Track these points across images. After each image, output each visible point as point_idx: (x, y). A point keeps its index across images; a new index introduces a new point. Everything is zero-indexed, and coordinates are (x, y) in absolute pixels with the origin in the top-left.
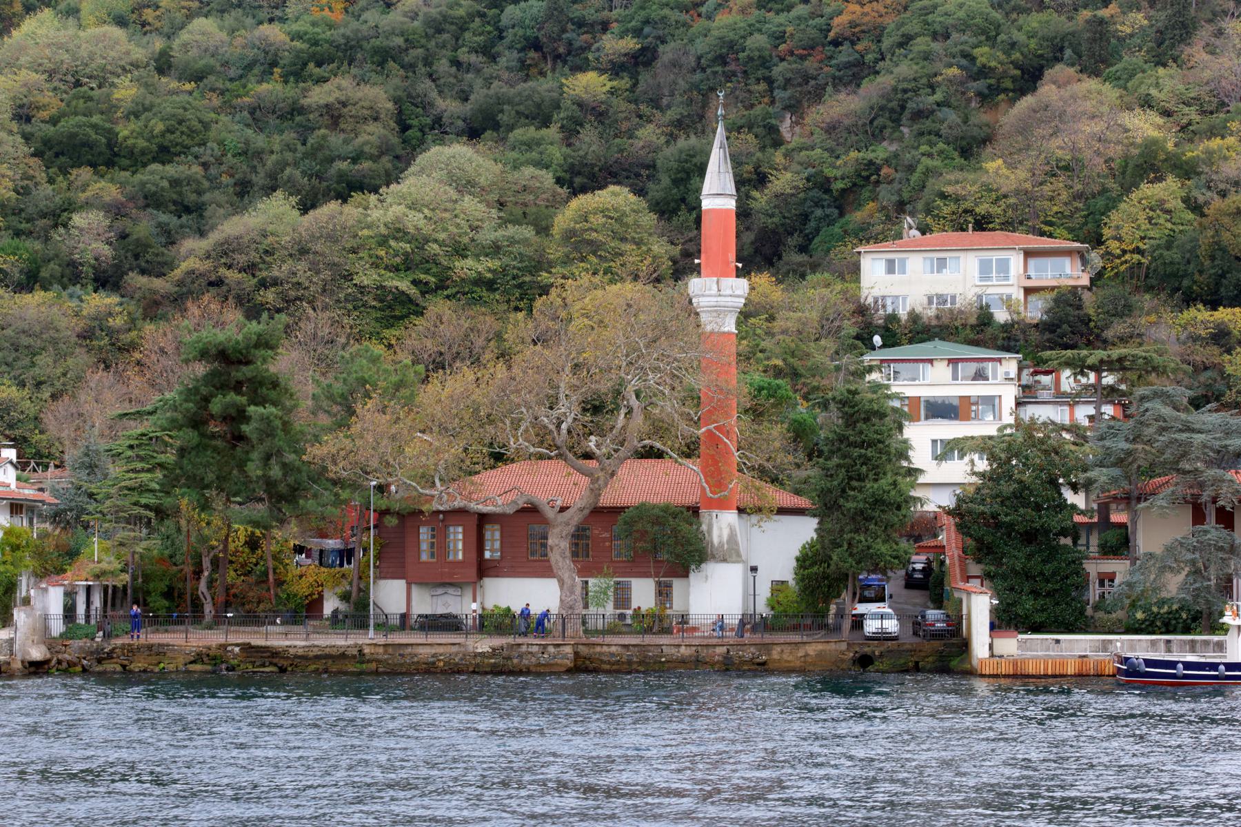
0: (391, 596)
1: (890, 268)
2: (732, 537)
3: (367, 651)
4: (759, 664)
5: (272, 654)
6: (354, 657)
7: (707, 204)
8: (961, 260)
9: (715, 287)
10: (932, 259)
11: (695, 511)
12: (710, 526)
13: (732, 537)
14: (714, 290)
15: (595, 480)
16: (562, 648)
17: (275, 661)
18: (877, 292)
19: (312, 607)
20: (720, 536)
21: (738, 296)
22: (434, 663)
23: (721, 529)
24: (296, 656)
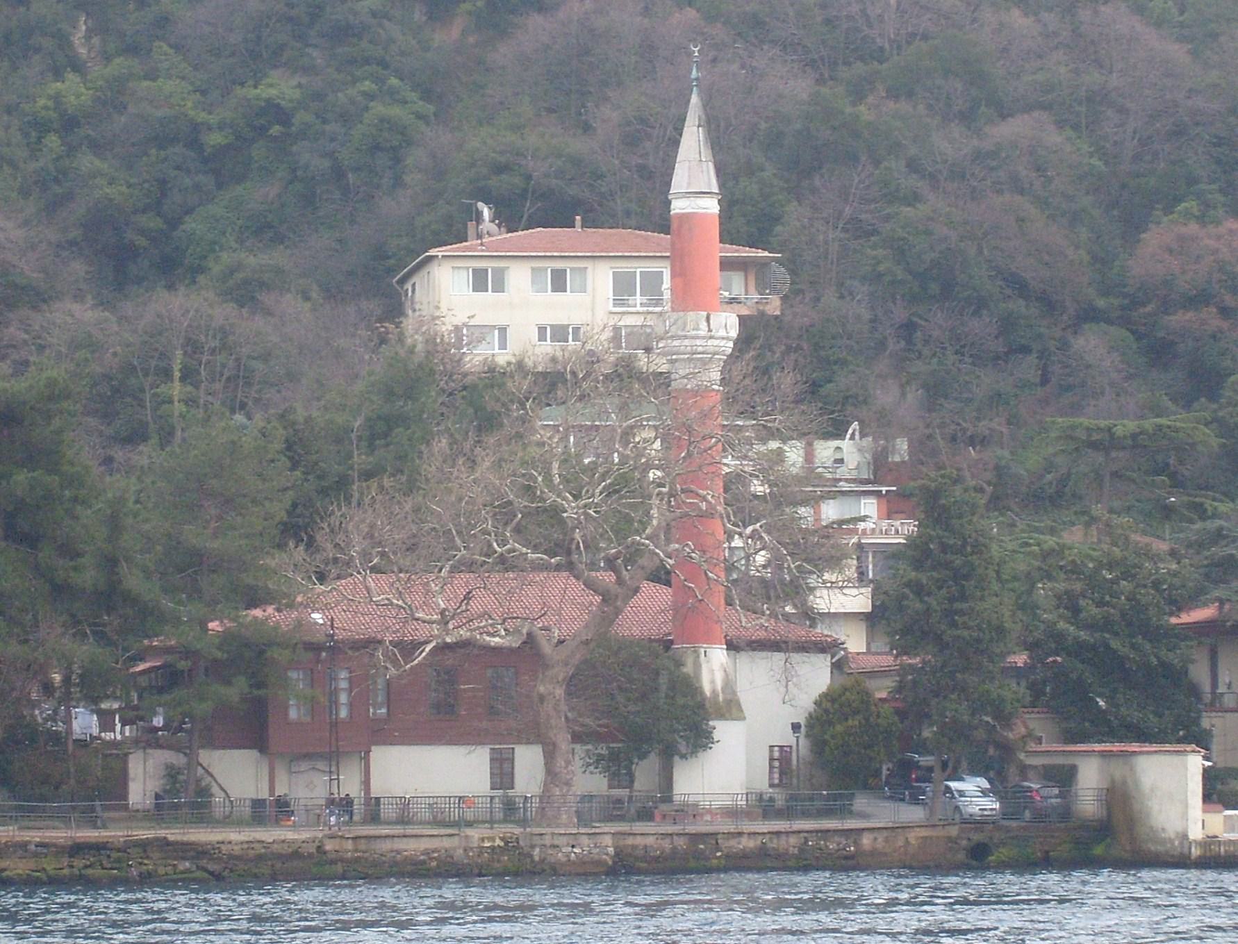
0: (237, 774)
1: (480, 281)
2: (729, 685)
3: (329, 846)
4: (846, 858)
5: (199, 852)
6: (310, 856)
7: (679, 206)
8: (590, 271)
9: (704, 325)
10: (468, 268)
11: (668, 645)
12: (697, 666)
13: (729, 685)
14: (703, 331)
15: (607, 598)
16: (599, 839)
17: (204, 863)
18: (460, 319)
19: (115, 788)
20: (713, 682)
21: (728, 339)
22: (424, 862)
23: (712, 671)
24: (231, 857)
